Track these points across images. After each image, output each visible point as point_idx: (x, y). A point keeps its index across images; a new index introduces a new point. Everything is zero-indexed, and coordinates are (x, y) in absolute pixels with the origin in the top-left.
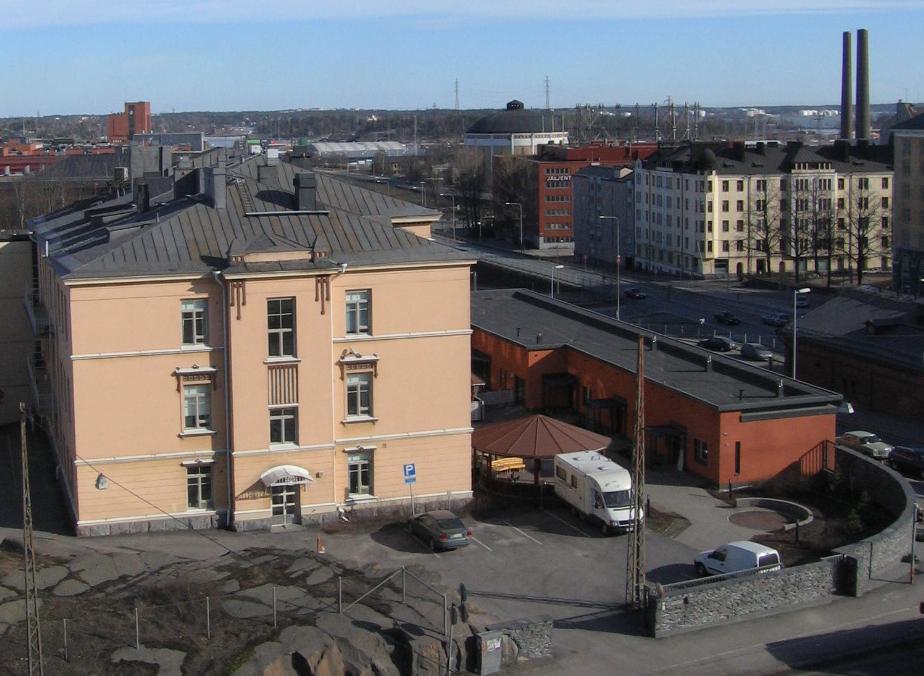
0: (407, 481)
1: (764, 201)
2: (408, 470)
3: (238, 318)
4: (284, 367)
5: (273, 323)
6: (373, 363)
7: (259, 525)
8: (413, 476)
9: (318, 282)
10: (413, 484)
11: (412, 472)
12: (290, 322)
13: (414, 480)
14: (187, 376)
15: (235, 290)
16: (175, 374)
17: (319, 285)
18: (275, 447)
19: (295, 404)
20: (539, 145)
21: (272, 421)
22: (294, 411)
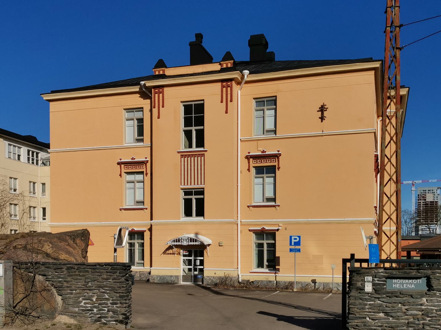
0: (291, 250)
1: (15, 263)
2: (293, 241)
3: (159, 118)
4: (194, 156)
5: (188, 122)
6: (276, 156)
7: (169, 280)
8: (297, 247)
9: (223, 87)
10: (297, 253)
11: (298, 243)
12: (200, 121)
13: (299, 250)
14: (125, 163)
15: (157, 95)
16: (118, 164)
17: (224, 89)
18: (189, 219)
19: (202, 186)
20: (191, 257)
21: (194, 195)
22: (201, 192)
